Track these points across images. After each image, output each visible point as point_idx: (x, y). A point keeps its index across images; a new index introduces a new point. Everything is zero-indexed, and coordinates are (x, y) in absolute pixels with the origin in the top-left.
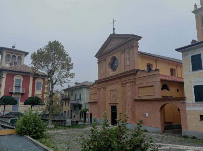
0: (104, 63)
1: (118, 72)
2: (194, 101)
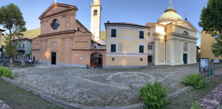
0: (46, 24)
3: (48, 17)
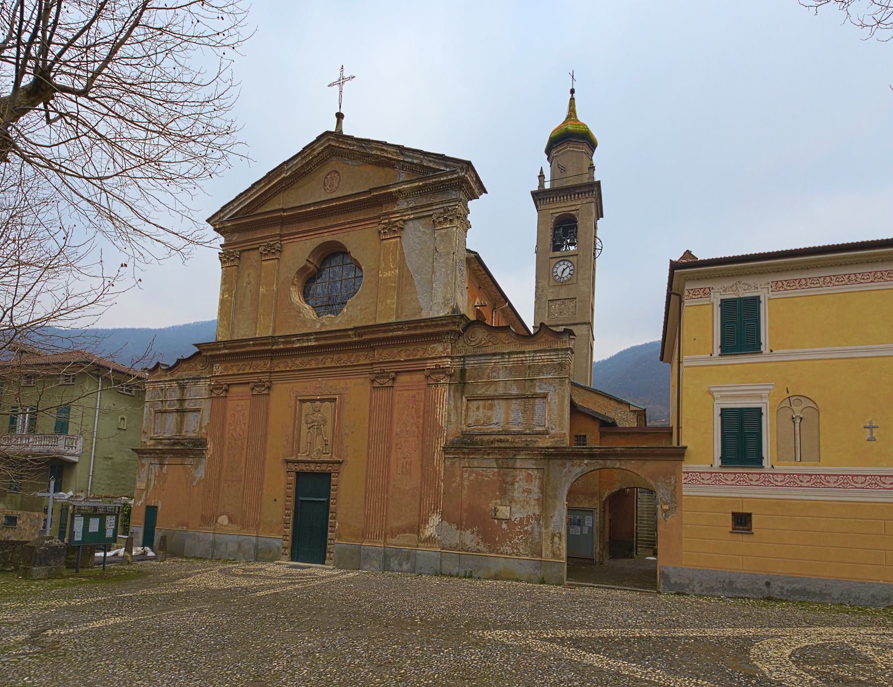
1: (353, 315)
2: (718, 462)
3: (283, 222)
